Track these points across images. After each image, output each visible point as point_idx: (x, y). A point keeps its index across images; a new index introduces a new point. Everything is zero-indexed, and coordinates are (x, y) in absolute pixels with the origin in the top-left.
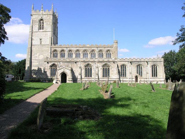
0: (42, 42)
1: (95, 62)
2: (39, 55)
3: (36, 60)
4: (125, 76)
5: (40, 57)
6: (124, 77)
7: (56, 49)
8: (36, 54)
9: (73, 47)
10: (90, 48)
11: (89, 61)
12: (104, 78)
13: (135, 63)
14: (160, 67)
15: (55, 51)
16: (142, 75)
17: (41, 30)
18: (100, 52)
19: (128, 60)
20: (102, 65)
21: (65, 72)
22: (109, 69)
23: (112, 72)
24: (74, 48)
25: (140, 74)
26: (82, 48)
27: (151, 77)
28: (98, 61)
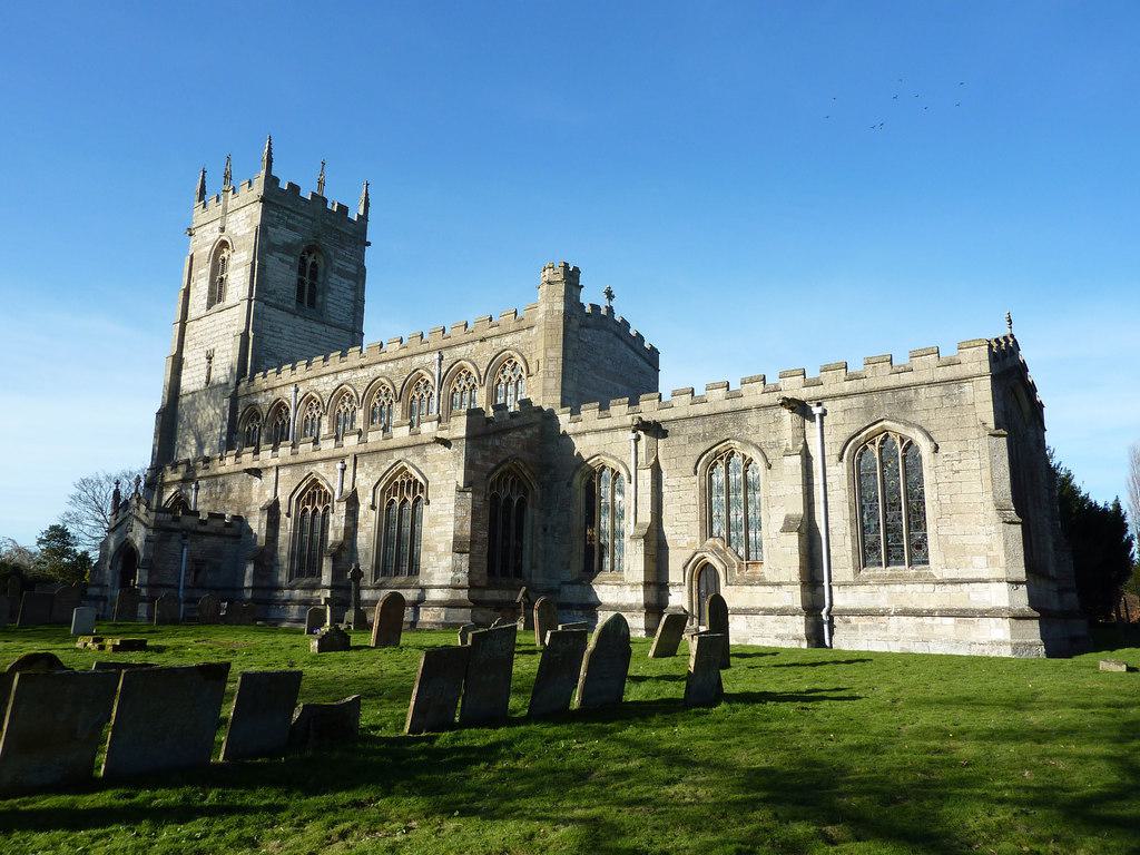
26: (361, 373)
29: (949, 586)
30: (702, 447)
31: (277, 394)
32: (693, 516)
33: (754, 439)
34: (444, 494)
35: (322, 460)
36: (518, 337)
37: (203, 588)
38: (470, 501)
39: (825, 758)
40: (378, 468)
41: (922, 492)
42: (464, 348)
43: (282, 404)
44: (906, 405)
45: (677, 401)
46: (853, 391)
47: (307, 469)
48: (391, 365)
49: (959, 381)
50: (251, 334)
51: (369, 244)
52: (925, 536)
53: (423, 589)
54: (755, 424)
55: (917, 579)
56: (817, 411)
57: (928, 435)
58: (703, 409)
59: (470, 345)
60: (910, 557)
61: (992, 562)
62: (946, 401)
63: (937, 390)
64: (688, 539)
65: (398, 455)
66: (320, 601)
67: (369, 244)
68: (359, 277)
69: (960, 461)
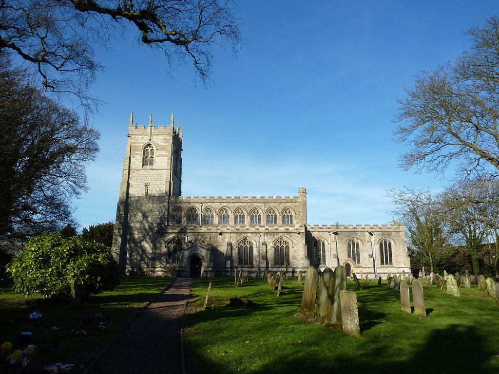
6: (385, 265)
9: (215, 201)
10: (249, 204)
11: (248, 231)
16: (359, 261)
18: (207, 212)
20: (274, 239)
24: (216, 204)
28: (267, 231)
30: (347, 239)
31: (192, 205)
32: (346, 253)
33: (359, 238)
36: (292, 204)
39: (475, 297)
40: (274, 237)
42: (273, 204)
43: (193, 208)
44: (390, 235)
45: (340, 227)
47: (243, 235)
48: (245, 204)
49: (399, 232)
50: (172, 182)
51: (182, 150)
53: (294, 268)
55: (392, 267)
56: (373, 234)
57: (394, 241)
58: (347, 230)
61: (405, 264)
63: (395, 233)
65: (280, 234)
67: (182, 150)
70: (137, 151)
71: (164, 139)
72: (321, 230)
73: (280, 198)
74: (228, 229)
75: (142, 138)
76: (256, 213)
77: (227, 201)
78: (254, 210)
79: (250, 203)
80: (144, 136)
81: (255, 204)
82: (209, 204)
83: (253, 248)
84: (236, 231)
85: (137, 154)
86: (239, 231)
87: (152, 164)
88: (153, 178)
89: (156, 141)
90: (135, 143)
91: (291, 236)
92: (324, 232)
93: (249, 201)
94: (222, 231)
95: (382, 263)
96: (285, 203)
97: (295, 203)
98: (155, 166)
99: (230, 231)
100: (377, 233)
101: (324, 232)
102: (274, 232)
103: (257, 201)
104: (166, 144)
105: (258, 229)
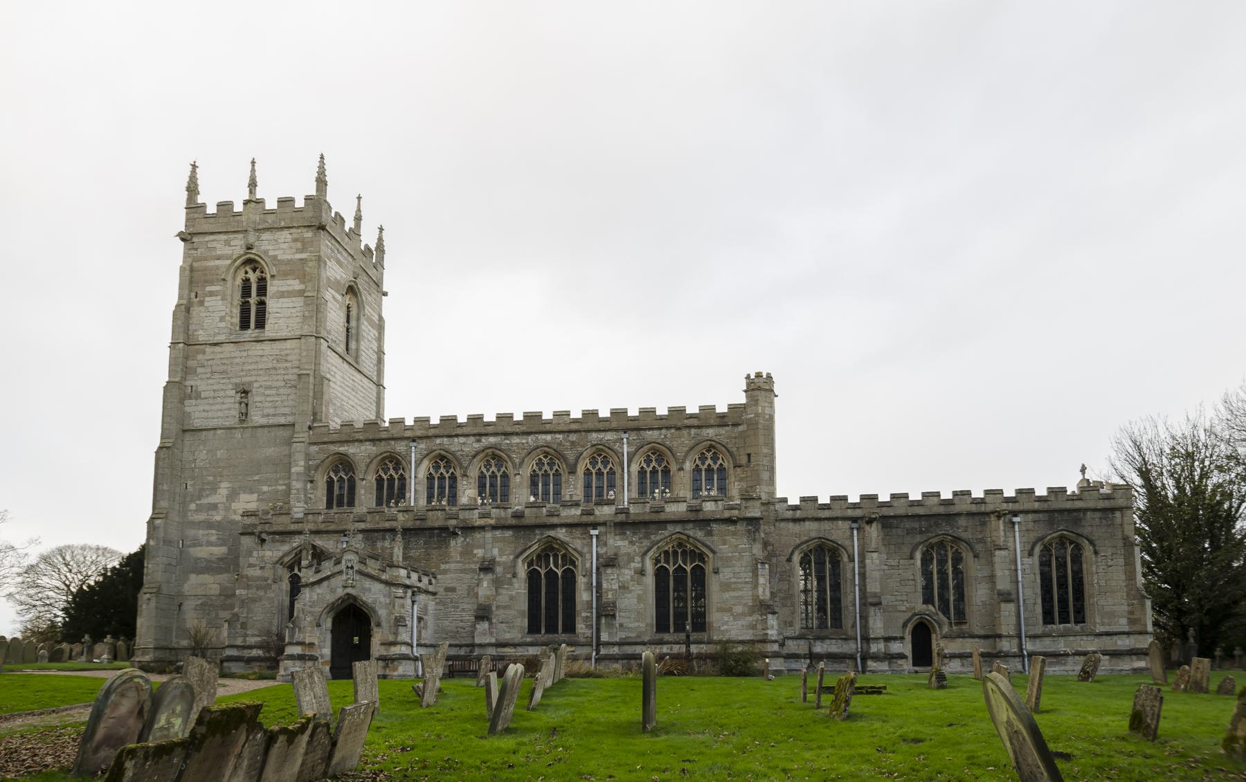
0: (252, 411)
1: (595, 525)
2: (233, 495)
3: (209, 525)
4: (565, 631)
5: (234, 506)
7: (342, 449)
8: (214, 490)
9: (459, 431)
10: (573, 437)
11: (555, 520)
12: (667, 637)
13: (910, 532)
14: (1106, 551)
15: (344, 464)
17: (251, 333)
18: (386, 471)
19: (298, 521)
21: (355, 598)
22: (570, 577)
23: (727, 595)
24: (462, 440)
25: (945, 609)
27: (1040, 629)
28: (622, 518)
29: (1104, 637)
34: (738, 564)
35: (562, 525)
36: (722, 431)
37: (1021, 649)
38: (768, 571)
41: (1082, 578)
42: (656, 433)
44: (1077, 522)
46: (1041, 509)
48: (560, 436)
49: (1113, 510)
51: (385, 294)
52: (1083, 605)
54: (964, 524)
55: (1084, 633)
59: (664, 431)
60: (1075, 618)
62: (1104, 521)
63: (1098, 515)
64: (908, 605)
66: (450, 665)
67: (385, 294)
68: (380, 326)
69: (1112, 560)
70: (212, 283)
71: (295, 240)
72: (826, 514)
73: (681, 411)
74: (482, 516)
75: (227, 243)
76: (600, 465)
77: (500, 429)
78: (396, 461)
79: (575, 431)
80: (232, 236)
81: (594, 435)
82: (438, 441)
83: (574, 577)
84: (514, 522)
85: (211, 294)
86: (526, 521)
87: (261, 324)
88: (261, 366)
89: (270, 247)
90: (206, 259)
91: (710, 534)
92: (837, 519)
93: (574, 427)
94: (464, 520)
95: (1048, 618)
96: (699, 427)
97: (736, 425)
98: (270, 330)
99: (492, 522)
100: (1030, 517)
101: (837, 519)
102: (647, 518)
103: (601, 426)
104: (304, 256)
105: (590, 513)
